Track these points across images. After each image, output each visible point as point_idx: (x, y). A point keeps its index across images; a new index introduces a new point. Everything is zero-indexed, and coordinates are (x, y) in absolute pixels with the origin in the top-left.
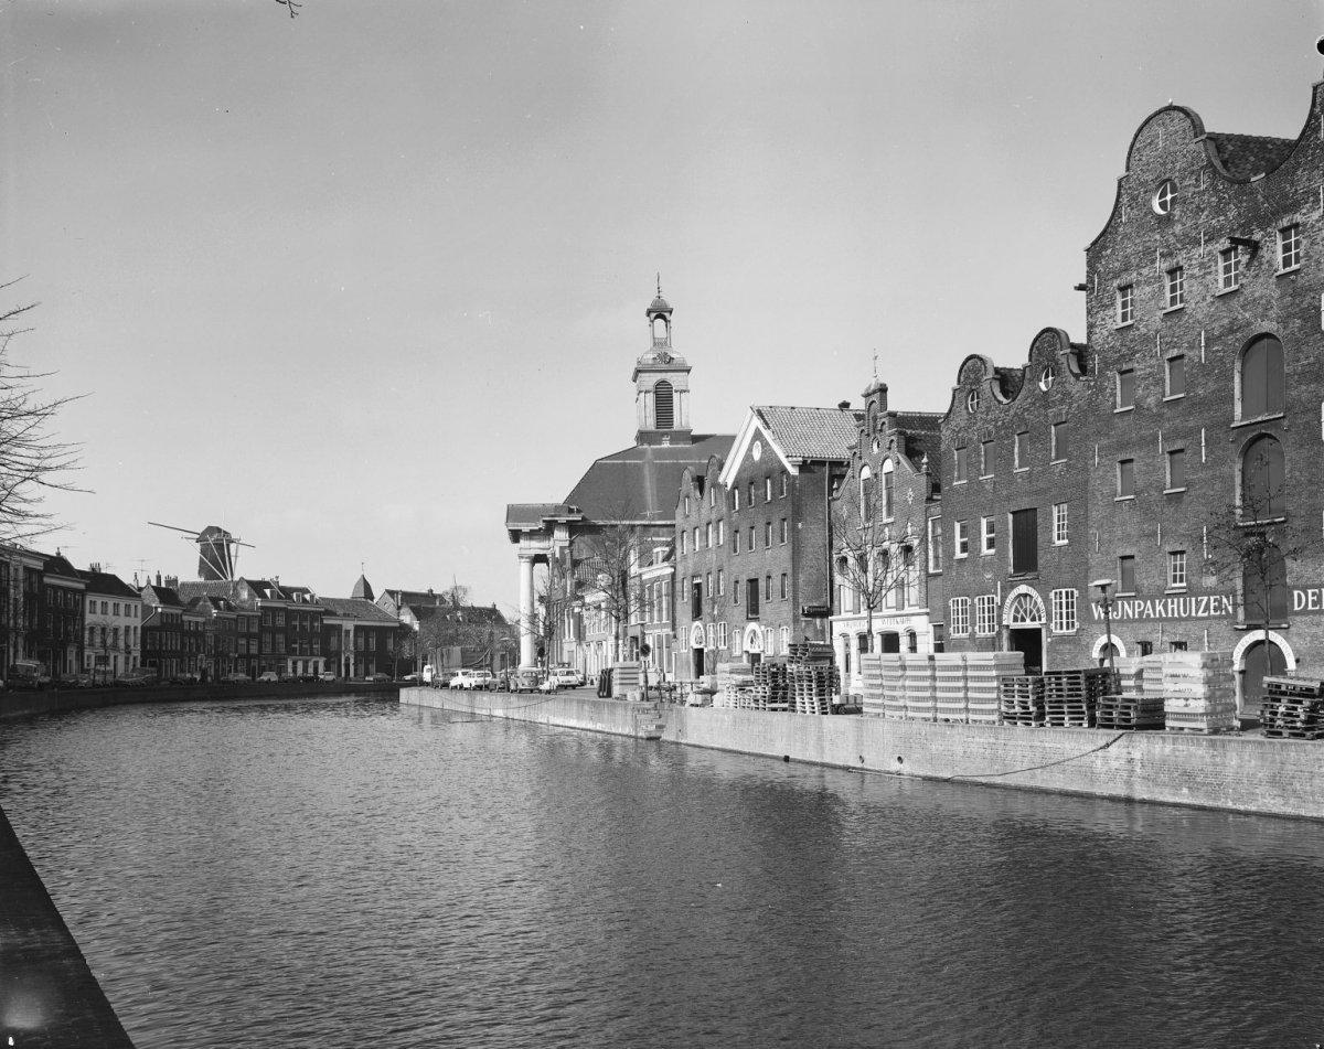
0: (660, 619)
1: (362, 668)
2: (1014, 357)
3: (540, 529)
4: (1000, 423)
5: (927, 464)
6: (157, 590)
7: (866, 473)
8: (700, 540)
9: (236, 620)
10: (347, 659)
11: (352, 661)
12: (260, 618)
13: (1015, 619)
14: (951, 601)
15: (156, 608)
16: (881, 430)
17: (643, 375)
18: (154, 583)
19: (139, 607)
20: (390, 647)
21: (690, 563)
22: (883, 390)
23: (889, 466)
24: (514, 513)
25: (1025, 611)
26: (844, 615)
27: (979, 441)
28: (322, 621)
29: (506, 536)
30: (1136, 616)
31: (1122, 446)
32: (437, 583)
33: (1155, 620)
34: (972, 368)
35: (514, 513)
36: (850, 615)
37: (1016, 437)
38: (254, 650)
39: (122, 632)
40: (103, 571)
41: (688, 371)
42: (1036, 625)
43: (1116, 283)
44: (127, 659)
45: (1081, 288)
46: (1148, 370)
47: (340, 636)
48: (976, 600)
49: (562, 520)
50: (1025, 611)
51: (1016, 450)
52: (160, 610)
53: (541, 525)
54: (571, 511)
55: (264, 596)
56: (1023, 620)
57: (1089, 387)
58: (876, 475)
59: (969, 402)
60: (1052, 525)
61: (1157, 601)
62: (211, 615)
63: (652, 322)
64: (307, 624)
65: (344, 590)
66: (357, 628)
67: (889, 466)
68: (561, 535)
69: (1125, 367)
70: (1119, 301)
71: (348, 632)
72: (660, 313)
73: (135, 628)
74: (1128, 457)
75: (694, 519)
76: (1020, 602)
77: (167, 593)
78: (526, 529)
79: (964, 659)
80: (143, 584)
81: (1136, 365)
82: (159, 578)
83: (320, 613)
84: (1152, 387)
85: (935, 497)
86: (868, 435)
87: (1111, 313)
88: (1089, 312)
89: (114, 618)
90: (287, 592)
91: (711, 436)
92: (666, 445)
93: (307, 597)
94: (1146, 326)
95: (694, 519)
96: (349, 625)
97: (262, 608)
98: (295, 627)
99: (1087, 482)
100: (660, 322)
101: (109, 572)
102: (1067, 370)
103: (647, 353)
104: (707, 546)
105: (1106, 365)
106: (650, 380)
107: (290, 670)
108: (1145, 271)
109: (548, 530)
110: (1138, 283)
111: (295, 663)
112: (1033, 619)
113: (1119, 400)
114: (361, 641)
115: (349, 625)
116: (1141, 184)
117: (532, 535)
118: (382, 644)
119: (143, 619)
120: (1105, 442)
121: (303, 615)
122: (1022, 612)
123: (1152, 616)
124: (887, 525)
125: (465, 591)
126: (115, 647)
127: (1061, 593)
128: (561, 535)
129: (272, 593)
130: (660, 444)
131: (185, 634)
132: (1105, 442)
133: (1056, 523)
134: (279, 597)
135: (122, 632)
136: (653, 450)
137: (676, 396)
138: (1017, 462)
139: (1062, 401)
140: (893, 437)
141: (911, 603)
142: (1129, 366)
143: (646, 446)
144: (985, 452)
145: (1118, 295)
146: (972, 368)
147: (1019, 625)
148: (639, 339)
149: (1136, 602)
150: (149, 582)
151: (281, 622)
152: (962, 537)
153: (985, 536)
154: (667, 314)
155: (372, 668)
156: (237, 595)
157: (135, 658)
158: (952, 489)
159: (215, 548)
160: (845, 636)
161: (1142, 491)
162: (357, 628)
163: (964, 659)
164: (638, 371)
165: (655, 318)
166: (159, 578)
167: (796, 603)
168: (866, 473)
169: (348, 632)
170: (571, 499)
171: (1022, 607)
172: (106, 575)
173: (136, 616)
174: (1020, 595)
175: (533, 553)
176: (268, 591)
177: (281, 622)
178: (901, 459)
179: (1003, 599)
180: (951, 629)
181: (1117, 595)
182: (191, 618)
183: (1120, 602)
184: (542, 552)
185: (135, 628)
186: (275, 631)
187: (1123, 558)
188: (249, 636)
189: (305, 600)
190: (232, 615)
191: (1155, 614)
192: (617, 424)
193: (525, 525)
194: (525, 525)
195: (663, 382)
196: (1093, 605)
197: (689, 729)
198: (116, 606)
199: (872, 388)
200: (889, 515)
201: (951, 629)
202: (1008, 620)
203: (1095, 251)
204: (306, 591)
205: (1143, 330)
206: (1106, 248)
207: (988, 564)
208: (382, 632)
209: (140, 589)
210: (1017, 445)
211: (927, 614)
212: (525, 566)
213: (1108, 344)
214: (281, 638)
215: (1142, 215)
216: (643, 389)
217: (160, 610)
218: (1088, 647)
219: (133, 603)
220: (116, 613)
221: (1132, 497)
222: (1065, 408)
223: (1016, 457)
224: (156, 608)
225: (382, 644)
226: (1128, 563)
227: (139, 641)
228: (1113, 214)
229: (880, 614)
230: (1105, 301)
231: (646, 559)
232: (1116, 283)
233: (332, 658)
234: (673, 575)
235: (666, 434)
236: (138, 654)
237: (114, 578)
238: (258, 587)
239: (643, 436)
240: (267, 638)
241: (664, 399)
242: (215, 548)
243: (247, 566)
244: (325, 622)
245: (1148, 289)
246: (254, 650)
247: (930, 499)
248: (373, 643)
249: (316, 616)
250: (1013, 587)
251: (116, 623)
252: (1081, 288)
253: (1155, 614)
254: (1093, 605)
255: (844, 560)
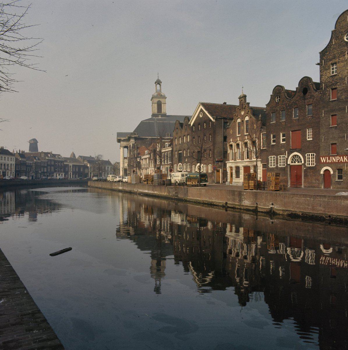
0: (167, 162)
1: (74, 176)
2: (292, 85)
3: (126, 139)
4: (287, 105)
5: (261, 117)
6: (19, 154)
7: (239, 120)
8: (181, 141)
9: (41, 163)
10: (70, 173)
11: (72, 174)
12: (47, 162)
13: (292, 162)
14: (306, 155)
15: (19, 159)
16: (245, 108)
17: (154, 99)
18: (18, 152)
19: (15, 159)
20: (82, 170)
21: (178, 147)
22: (245, 97)
23: (247, 118)
24: (119, 134)
25: (296, 160)
26: (231, 161)
27: (280, 110)
28: (64, 163)
29: (116, 140)
30: (337, 161)
31: (333, 111)
32: (93, 154)
33: (344, 162)
34: (278, 91)
35: (119, 134)
36: (240, 161)
37: (293, 109)
38: (45, 171)
39: (10, 165)
40: (4, 149)
41: (166, 98)
42: (300, 164)
43: (330, 62)
44: (11, 173)
45: (318, 64)
46: (342, 88)
47: (68, 167)
48: (278, 157)
49: (133, 136)
50: (296, 160)
51: (293, 113)
52: (20, 159)
53: (127, 138)
54: (135, 134)
55: (48, 156)
56: (295, 162)
57: (320, 93)
58: (243, 121)
59: (276, 99)
60: (306, 134)
61: (345, 157)
62: (34, 161)
63: (156, 85)
64: (60, 164)
65: (68, 156)
66: (73, 165)
67: (247, 118)
68: (132, 141)
69: (334, 87)
70: (331, 68)
71: (70, 166)
72: (158, 82)
73: (13, 164)
74: (334, 114)
75: (179, 134)
76: (294, 157)
77: (22, 155)
78: (122, 139)
79: (49, 169)
80: (15, 152)
81: (338, 87)
82: (20, 151)
83: (63, 161)
84: (343, 93)
85: (263, 127)
86: (240, 109)
87: (329, 71)
88: (320, 71)
89: (8, 161)
90: (54, 155)
91: (170, 116)
92: (160, 117)
93: (60, 157)
94: (341, 75)
95: (179, 134)
96: (71, 164)
97: (47, 159)
98: (57, 165)
99: (319, 122)
100: (158, 85)
101: (6, 149)
102: (312, 88)
103: (155, 93)
104: (184, 142)
105: (327, 87)
106: (156, 100)
107: (55, 176)
108: (341, 59)
109: (129, 140)
110: (339, 62)
111: (56, 174)
112: (299, 162)
113: (331, 97)
114: (74, 169)
115: (71, 164)
116: (340, 32)
117: (124, 140)
118: (79, 170)
119: (15, 162)
120: (326, 109)
121: (59, 162)
122: (294, 160)
123: (343, 161)
124: (246, 135)
125: (102, 156)
126: (8, 169)
127: (272, 157)
128: (132, 141)
129: (50, 155)
130: (158, 117)
131: (27, 166)
132: (326, 109)
133: (308, 134)
134: (52, 157)
135: (10, 165)
136: (157, 119)
137: (162, 105)
138: (293, 116)
139: (310, 98)
140: (249, 110)
141: (238, 159)
142: (335, 87)
143: (154, 118)
144: (282, 113)
145: (331, 66)
146: (278, 91)
147: (293, 164)
148: (152, 90)
149: (337, 157)
150: (17, 152)
151: (53, 163)
152: (283, 137)
153: (281, 138)
154: (160, 83)
155: (77, 176)
156: (41, 156)
157: (13, 172)
158: (270, 124)
159: (34, 144)
160: (231, 168)
161: (339, 124)
162: (73, 165)
163: (49, 169)
164: (152, 98)
165: (157, 84)
166: (20, 151)
167: (214, 159)
168: (239, 120)
169: (70, 166)
170: (135, 131)
171: (294, 159)
172: (5, 150)
173: (13, 161)
174: (294, 155)
175: (124, 145)
176: (49, 155)
177: (53, 163)
178: (252, 116)
179: (288, 156)
180: (269, 165)
181: (330, 155)
182: (29, 162)
183: (331, 157)
184: (126, 145)
185: (13, 164)
186: (51, 166)
187: (332, 144)
188: (44, 167)
189: (59, 158)
190: (40, 161)
191: (344, 160)
192: (146, 112)
193: (122, 138)
194: (122, 138)
195: (159, 101)
196: (321, 158)
197: (189, 194)
198: (5, 158)
199: (242, 96)
200: (238, 134)
201: (269, 165)
202: (289, 162)
203: (323, 54)
204: (59, 155)
205: (340, 76)
206: (327, 52)
207: (283, 145)
208: (79, 167)
209: (15, 154)
210: (294, 111)
211: (260, 161)
212: (122, 149)
213: (327, 80)
214: (52, 168)
215: (340, 42)
216: (154, 102)
217: (20, 159)
218: (320, 171)
219: (13, 157)
220: (8, 160)
221: (336, 126)
222: (311, 100)
223: (293, 115)
224: (19, 159)
225: (79, 170)
226: (334, 146)
227: (14, 167)
228: (330, 42)
229: (229, 162)
230: (327, 68)
231: (163, 146)
232: (330, 62)
233: (66, 173)
234: (172, 151)
235: (160, 115)
236: (14, 171)
237: (7, 150)
238: (46, 154)
239: (153, 115)
240: (49, 167)
241: (159, 106)
242: (34, 144)
243: (42, 148)
244: (64, 163)
245: (342, 64)
246: (45, 171)
247: (261, 128)
248: (77, 170)
249: (62, 162)
250: (292, 153)
251: (8, 163)
252: (318, 64)
253: (344, 160)
254: (321, 158)
255: (231, 146)
